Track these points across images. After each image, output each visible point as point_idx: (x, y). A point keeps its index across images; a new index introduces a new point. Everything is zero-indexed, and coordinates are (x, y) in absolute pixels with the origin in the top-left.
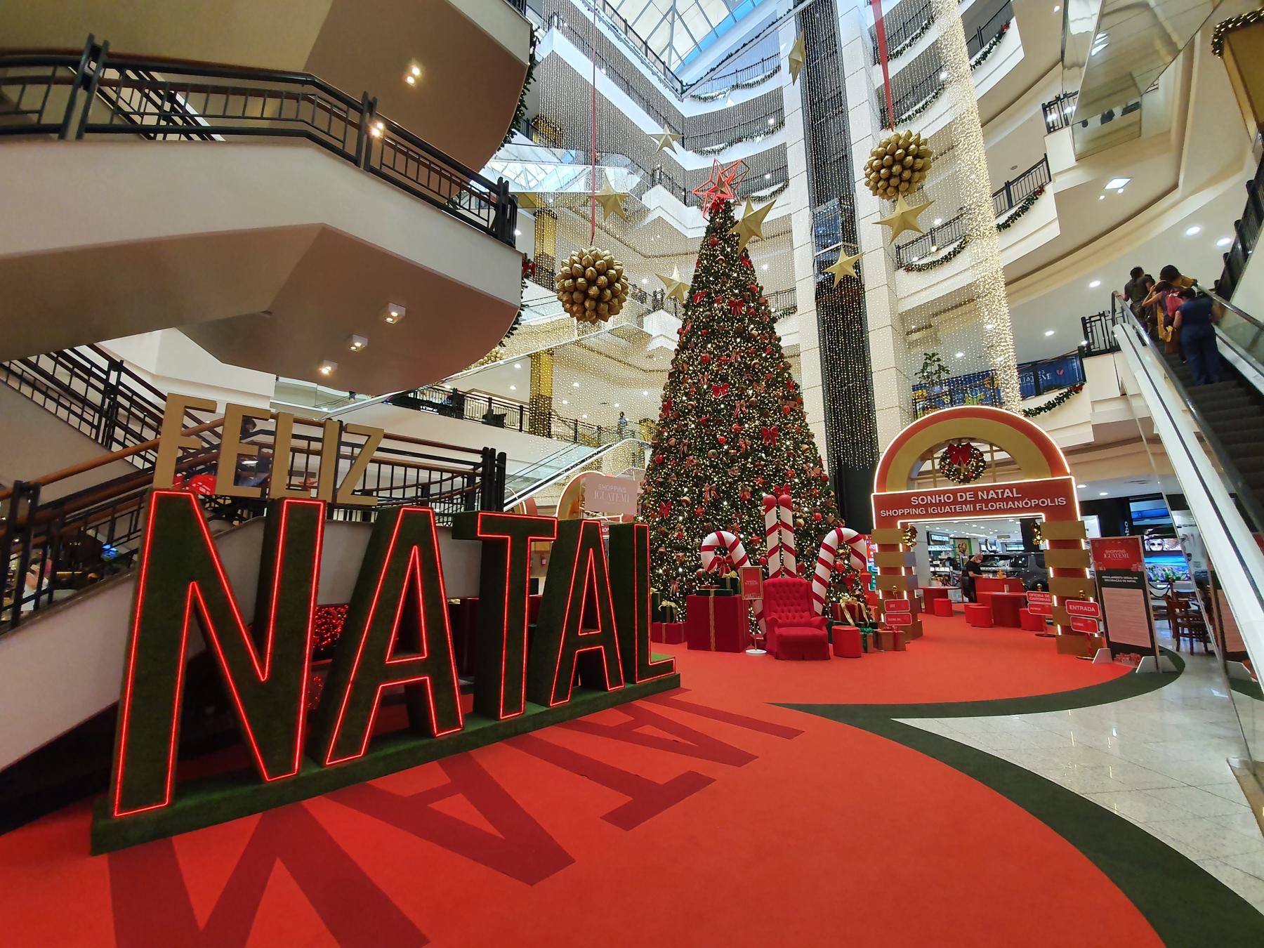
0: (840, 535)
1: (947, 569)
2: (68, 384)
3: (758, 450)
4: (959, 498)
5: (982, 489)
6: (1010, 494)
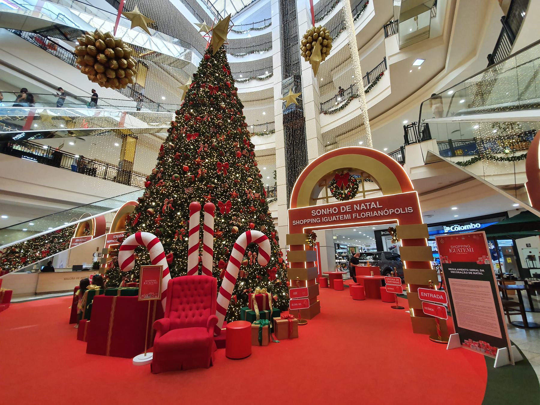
0: (249, 236)
1: (345, 261)
3: (212, 177)
4: (343, 207)
6: (375, 206)
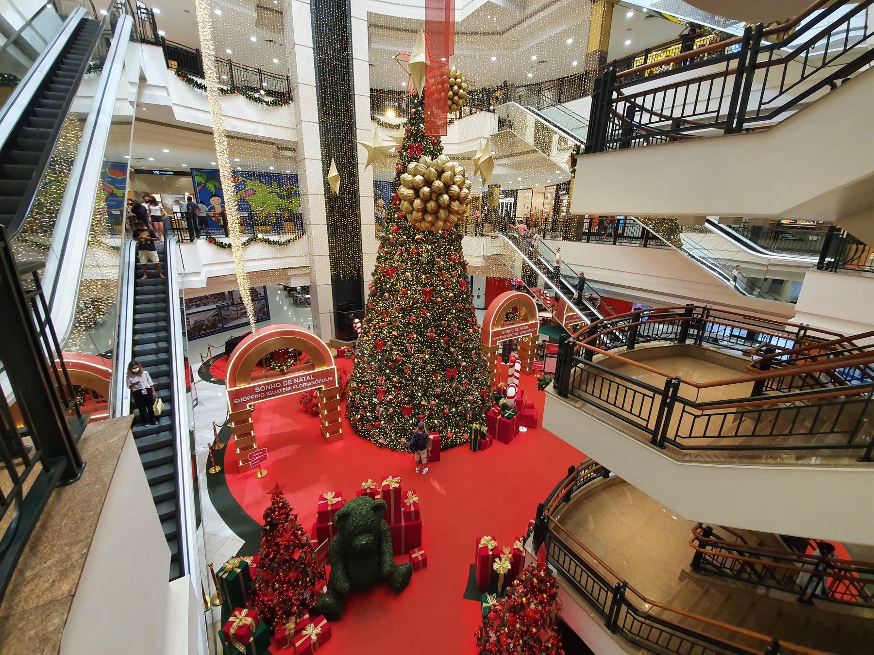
2: (734, 415)
5: (296, 378)
